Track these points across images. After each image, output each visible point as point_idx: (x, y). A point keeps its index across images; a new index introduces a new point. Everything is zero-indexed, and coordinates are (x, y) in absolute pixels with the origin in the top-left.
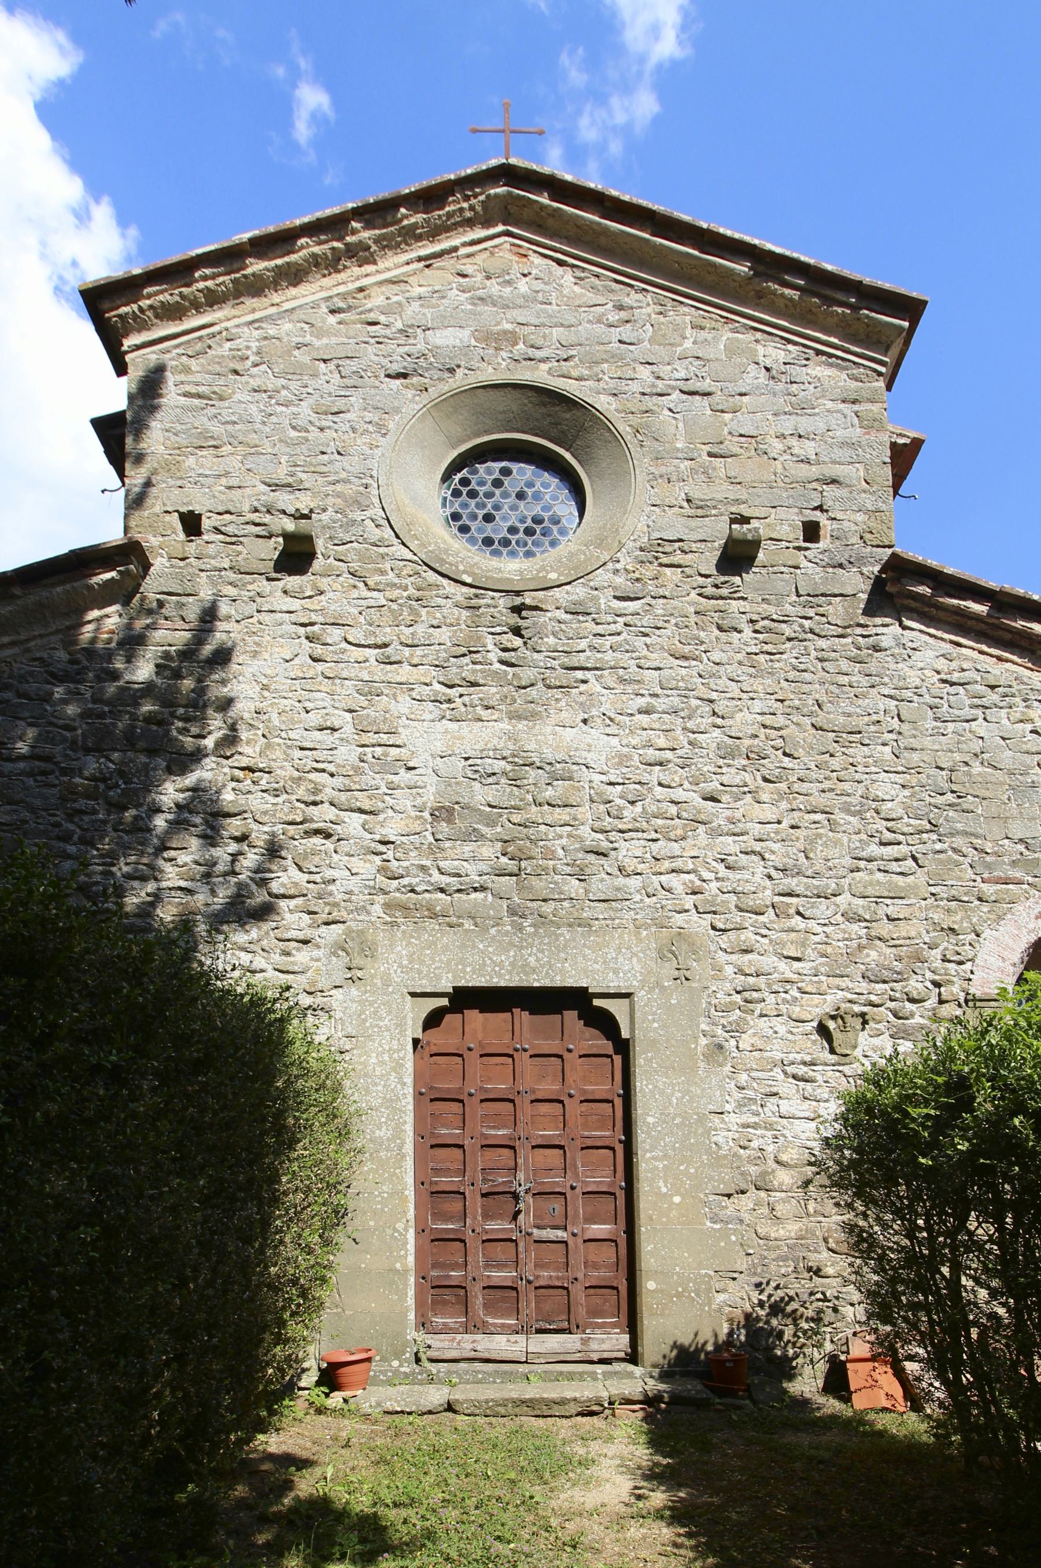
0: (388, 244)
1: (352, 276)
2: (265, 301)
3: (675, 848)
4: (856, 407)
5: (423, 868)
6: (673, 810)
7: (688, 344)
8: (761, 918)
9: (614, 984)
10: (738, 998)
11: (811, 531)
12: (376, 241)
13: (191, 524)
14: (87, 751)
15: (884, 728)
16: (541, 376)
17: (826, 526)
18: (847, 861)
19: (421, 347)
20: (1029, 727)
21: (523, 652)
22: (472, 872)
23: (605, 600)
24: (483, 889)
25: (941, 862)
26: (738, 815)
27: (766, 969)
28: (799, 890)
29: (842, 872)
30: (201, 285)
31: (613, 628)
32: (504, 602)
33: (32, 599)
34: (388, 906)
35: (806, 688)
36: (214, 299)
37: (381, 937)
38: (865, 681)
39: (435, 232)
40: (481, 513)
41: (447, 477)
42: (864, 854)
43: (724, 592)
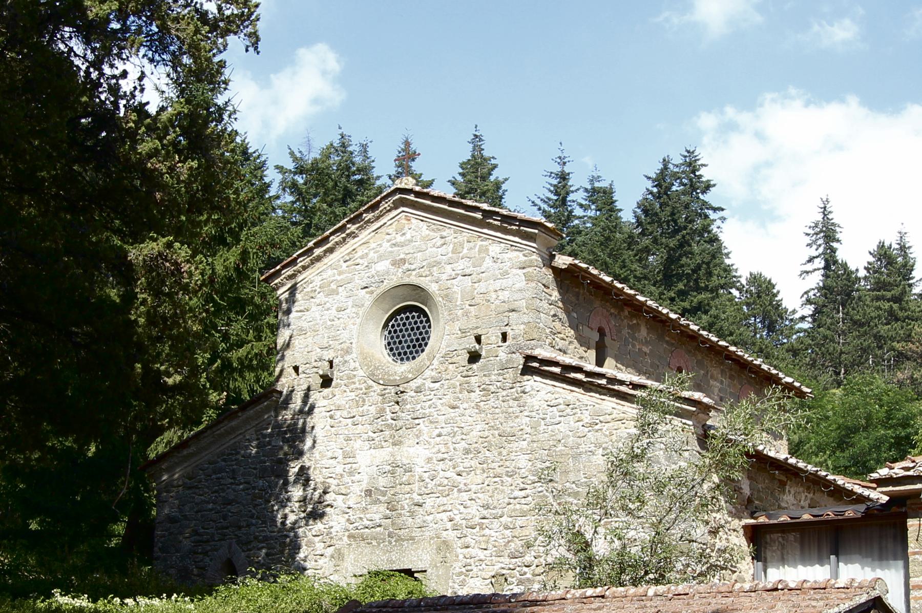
0: (361, 228)
1: (352, 242)
2: (322, 263)
3: (445, 500)
4: (524, 271)
5: (361, 518)
6: (446, 482)
7: (465, 251)
8: (474, 531)
9: (420, 566)
10: (464, 570)
11: (504, 337)
12: (357, 229)
13: (296, 369)
14: (260, 478)
15: (524, 432)
16: (413, 279)
17: (510, 334)
18: (507, 500)
19: (373, 272)
20: (581, 423)
21: (399, 413)
22: (377, 518)
23: (429, 384)
24: (380, 526)
25: (541, 497)
26: (468, 482)
27: (474, 555)
28: (488, 516)
29: (505, 505)
30: (300, 265)
31: (429, 397)
32: (393, 390)
33: (245, 416)
34: (349, 537)
35: (497, 416)
36: (305, 268)
37: (346, 552)
38: (518, 409)
39: (378, 218)
40: (407, 322)
41: (386, 325)
42: (512, 496)
43: (470, 373)
